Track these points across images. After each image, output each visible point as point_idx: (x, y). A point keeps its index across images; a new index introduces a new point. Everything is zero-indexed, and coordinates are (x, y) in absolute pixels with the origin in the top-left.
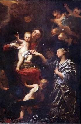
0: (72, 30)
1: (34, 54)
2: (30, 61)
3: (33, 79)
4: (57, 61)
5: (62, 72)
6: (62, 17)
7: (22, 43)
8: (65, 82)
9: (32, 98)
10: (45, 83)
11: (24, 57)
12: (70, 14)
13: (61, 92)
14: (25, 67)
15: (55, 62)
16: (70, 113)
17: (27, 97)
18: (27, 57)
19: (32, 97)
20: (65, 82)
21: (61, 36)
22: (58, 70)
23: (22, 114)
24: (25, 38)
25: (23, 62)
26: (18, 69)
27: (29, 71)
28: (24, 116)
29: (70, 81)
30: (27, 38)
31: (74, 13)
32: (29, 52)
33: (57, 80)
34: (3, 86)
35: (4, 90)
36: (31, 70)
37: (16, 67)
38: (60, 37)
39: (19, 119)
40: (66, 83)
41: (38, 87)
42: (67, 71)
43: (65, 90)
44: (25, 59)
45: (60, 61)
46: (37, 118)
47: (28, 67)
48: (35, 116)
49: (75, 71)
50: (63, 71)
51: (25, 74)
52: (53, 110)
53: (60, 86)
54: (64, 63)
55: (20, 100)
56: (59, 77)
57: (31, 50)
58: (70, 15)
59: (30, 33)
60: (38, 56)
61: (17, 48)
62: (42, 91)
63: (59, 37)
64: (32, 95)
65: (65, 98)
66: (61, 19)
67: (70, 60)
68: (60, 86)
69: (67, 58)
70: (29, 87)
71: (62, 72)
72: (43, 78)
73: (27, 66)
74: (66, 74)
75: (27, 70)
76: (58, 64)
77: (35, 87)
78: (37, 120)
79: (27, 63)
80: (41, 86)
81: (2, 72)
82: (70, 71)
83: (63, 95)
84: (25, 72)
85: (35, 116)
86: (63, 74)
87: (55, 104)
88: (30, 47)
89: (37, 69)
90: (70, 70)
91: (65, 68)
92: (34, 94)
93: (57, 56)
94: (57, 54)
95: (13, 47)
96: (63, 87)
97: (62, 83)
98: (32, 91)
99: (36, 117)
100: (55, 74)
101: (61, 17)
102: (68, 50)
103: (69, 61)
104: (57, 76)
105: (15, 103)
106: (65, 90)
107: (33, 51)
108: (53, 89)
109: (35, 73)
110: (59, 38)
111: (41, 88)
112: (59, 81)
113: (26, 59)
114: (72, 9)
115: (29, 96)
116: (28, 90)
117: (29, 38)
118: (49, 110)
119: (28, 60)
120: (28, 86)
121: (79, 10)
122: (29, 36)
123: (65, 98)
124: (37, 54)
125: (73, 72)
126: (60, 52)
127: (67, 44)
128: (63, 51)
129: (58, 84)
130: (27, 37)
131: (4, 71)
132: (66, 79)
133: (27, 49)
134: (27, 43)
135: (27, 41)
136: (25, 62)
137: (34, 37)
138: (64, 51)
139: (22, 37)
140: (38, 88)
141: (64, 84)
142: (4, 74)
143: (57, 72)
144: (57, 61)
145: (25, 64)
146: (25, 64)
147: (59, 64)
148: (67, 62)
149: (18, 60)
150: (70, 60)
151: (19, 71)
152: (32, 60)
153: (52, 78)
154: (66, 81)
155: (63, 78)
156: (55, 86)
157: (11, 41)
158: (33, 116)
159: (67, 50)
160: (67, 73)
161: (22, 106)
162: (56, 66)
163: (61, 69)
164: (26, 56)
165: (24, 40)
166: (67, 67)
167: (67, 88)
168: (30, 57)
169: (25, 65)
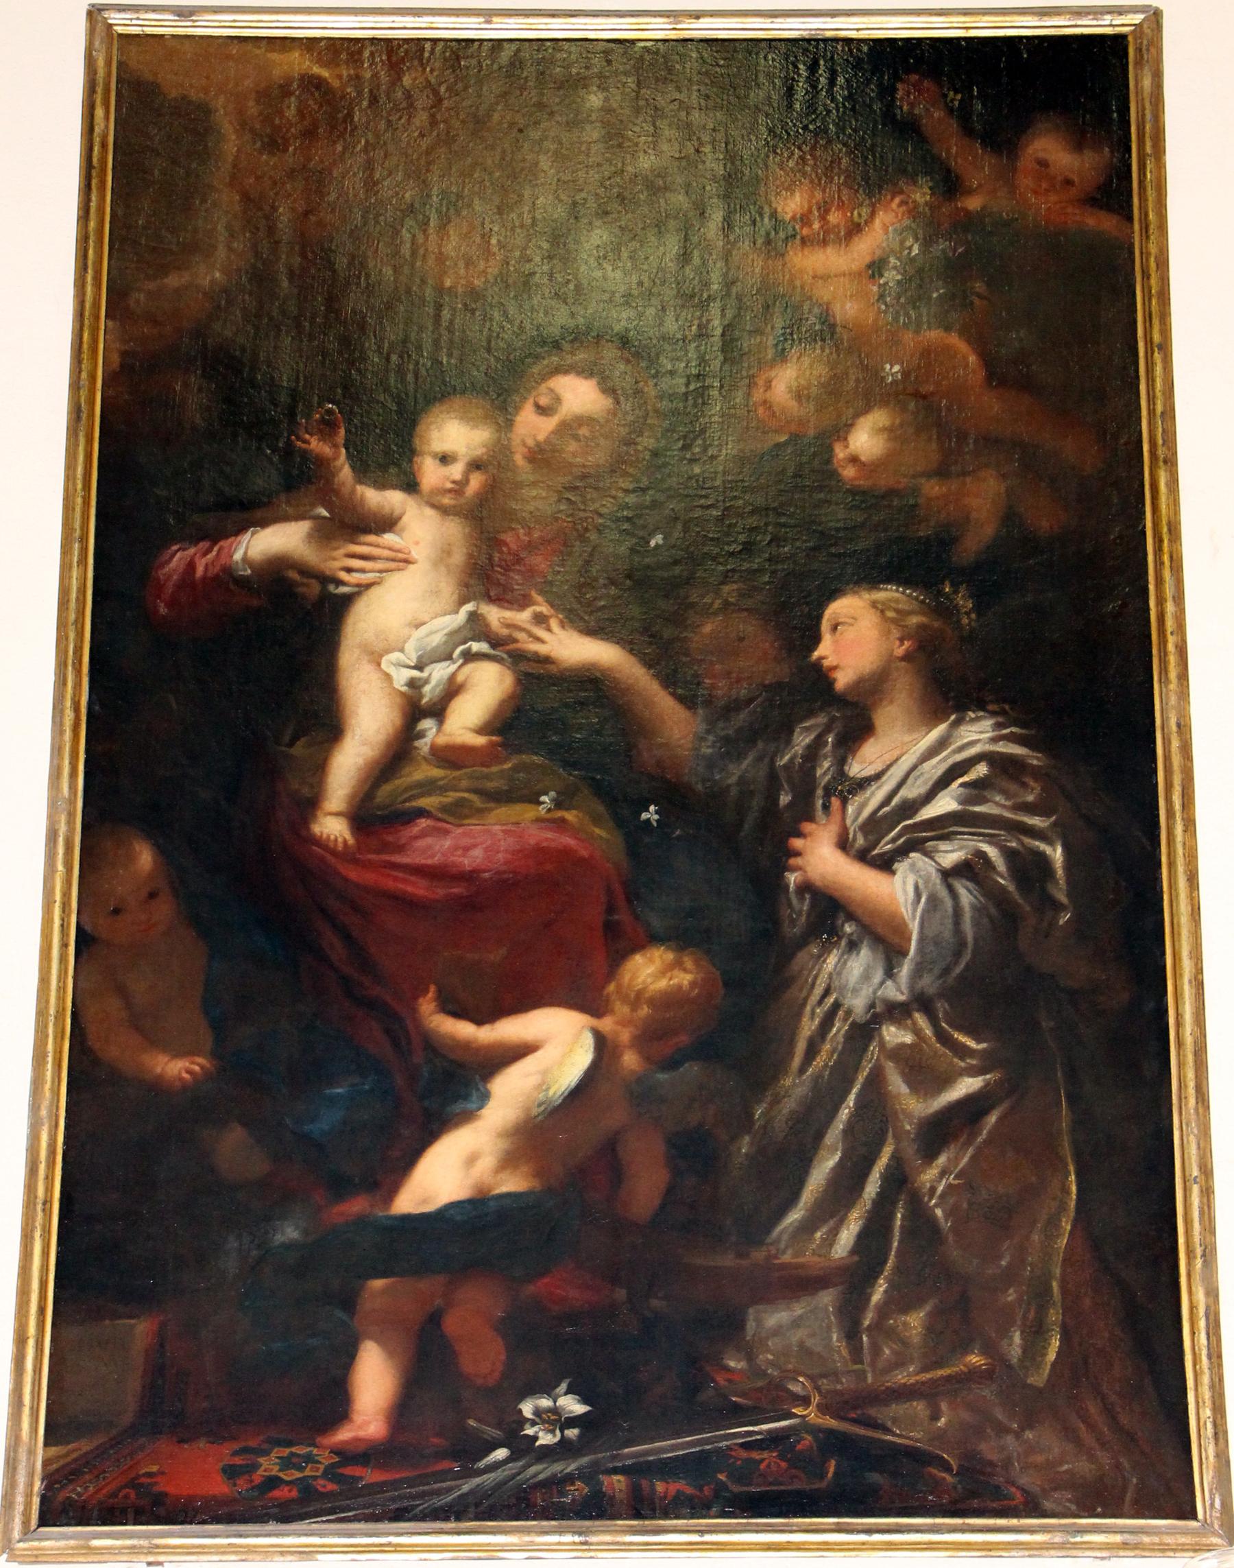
0: (999, 374)
1: (534, 647)
2: (480, 740)
3: (536, 940)
4: (828, 729)
5: (886, 864)
6: (877, 223)
7: (387, 523)
8: (928, 983)
9: (512, 1184)
10: (668, 1001)
11: (413, 684)
12: (969, 192)
13: (876, 1107)
14: (425, 802)
15: (802, 740)
16: (1004, 1362)
17: (448, 1171)
18: (453, 690)
19: (508, 1162)
20: (928, 983)
21: (866, 439)
22: (843, 844)
23: (374, 1381)
24: (431, 474)
25: (398, 751)
26: (332, 827)
27: (474, 858)
28: (402, 1411)
29: (759, 1101)
30: (456, 471)
31: (1025, 182)
32: (476, 627)
33: (821, 957)
34: (138, 1029)
35: (156, 1088)
36: (485, 841)
37: (311, 804)
38: (854, 460)
39: (338, 1451)
40: (941, 995)
41: (588, 1040)
42: (951, 854)
43: (923, 1072)
44: (417, 709)
45: (855, 721)
46: (572, 1433)
47: (458, 811)
48: (545, 1403)
49: (1057, 854)
50: (902, 852)
51: (418, 888)
52: (777, 1331)
53: (863, 1032)
54: (904, 753)
55: (357, 1206)
56: (851, 917)
57: (492, 600)
58: (973, 203)
59: (487, 418)
60: (591, 684)
61: (326, 579)
62: (641, 1095)
63: (840, 453)
64: (503, 1145)
65: (934, 1176)
66: (865, 247)
67: (988, 723)
68: (863, 1032)
69: (948, 695)
70: (467, 1046)
71: (886, 864)
72: (654, 939)
73: (452, 796)
74: (943, 893)
75: (447, 843)
76: (841, 774)
77: (555, 1048)
78: (564, 1449)
79: (450, 756)
80: (625, 1036)
81: (131, 858)
82: (992, 851)
83: (910, 1150)
84: (420, 871)
85: (545, 1403)
86: (900, 891)
87: (808, 1258)
88: (489, 571)
89: (574, 832)
90: (991, 839)
91: (928, 812)
92: (533, 1136)
93: (820, 677)
94: (825, 650)
95: (277, 577)
96: (908, 1039)
97: (897, 991)
98: (511, 1095)
99: (555, 1411)
100: (806, 887)
101: (855, 229)
102: (964, 602)
103: (978, 734)
104: (830, 913)
105: (290, 1246)
106: (923, 1072)
107: (523, 617)
108: (779, 1067)
109: (537, 883)
110: (849, 472)
111: (630, 1060)
112: (853, 977)
113: (438, 711)
114: (1001, 138)
115: (471, 1160)
116: (452, 1087)
117: (476, 465)
118: (729, 1326)
119: (465, 721)
120: (464, 1030)
121: (1078, 146)
122: (479, 452)
123: (934, 1176)
124: (573, 648)
125: (1029, 869)
126: (858, 633)
127: (945, 540)
128: (887, 616)
129: (837, 1006)
130: (445, 459)
131: (161, 851)
132: (943, 951)
133: (448, 589)
134: (455, 530)
135: (447, 500)
136: (423, 745)
137: (541, 456)
138: (914, 620)
139: (393, 459)
140: (583, 1057)
141: (922, 1002)
142: (152, 895)
143: (822, 858)
144: (828, 729)
145: (423, 772)
146: (423, 772)
147: (856, 769)
148: (942, 744)
149: (328, 725)
150: (988, 723)
151: (347, 856)
152: (509, 724)
153: (763, 935)
154: (946, 971)
155: (901, 929)
156: (808, 1027)
157: (252, 511)
158: (527, 1408)
159: (944, 611)
160: (947, 874)
161: (378, 1284)
162: (805, 798)
163: (875, 826)
164: (439, 673)
165: (411, 486)
166: (946, 803)
167: (962, 1051)
168: (486, 688)
169: (429, 787)
